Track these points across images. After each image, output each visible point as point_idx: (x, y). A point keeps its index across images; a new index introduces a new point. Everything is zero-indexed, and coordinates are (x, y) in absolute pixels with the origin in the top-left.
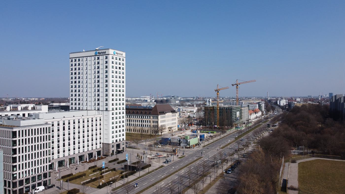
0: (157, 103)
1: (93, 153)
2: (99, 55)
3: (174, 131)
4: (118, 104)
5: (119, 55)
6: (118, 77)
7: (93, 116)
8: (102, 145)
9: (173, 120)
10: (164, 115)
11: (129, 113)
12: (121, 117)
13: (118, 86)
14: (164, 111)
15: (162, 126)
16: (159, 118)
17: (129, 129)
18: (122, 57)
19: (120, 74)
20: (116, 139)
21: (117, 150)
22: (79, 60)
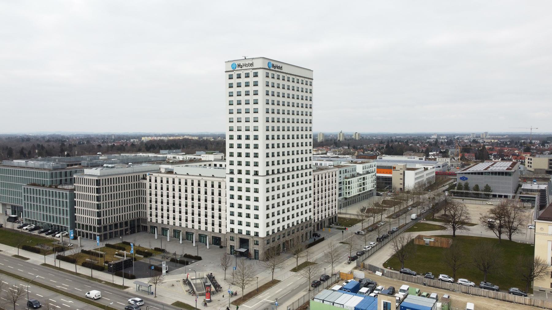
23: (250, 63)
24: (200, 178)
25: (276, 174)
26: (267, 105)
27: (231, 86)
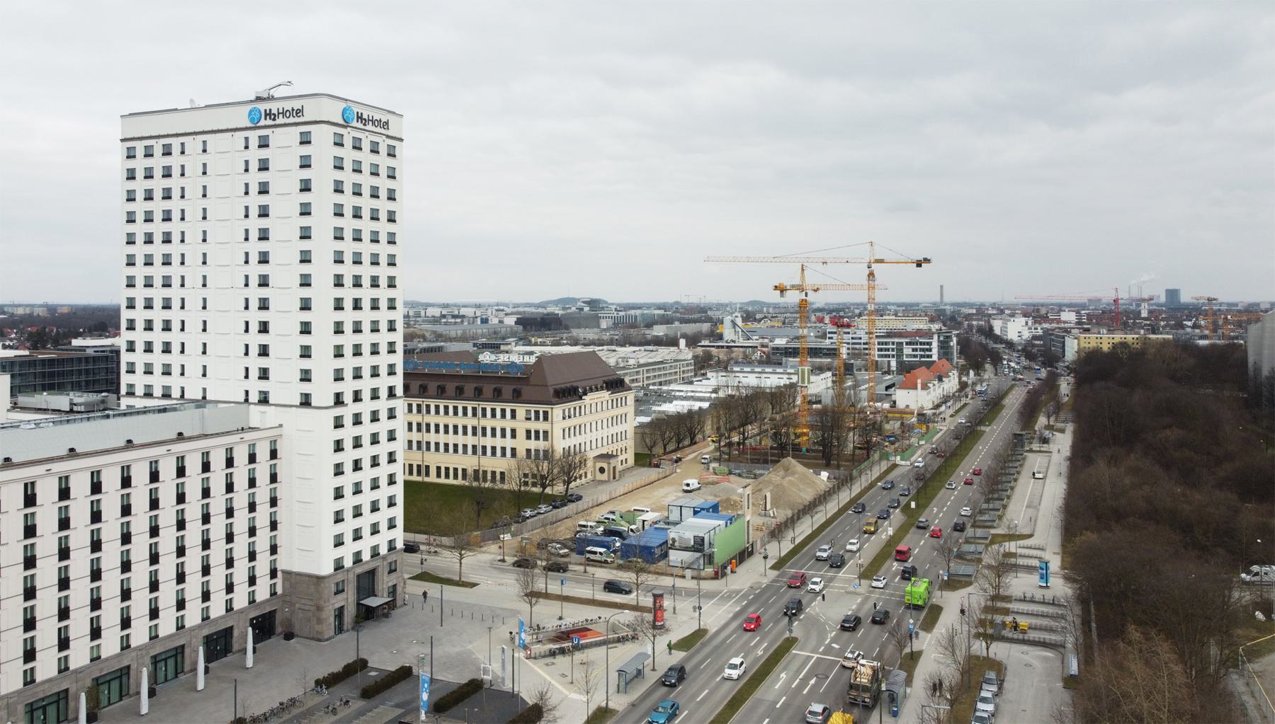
0: (525, 328)
1: (231, 628)
2: (269, 122)
3: (619, 468)
4: (366, 327)
5: (370, 127)
6: (366, 214)
7: (236, 438)
8: (284, 580)
9: (614, 420)
10: (577, 403)
11: (423, 392)
12: (383, 371)
13: (366, 259)
14: (575, 384)
15: (567, 453)
16: (555, 419)
17: (419, 466)
18: (388, 137)
19: (378, 175)
20: (357, 546)
21: (358, 604)
22: (167, 152)
23: (296, 109)
24: (179, 448)
25: (400, 397)
26: (338, 219)
27: (131, 176)
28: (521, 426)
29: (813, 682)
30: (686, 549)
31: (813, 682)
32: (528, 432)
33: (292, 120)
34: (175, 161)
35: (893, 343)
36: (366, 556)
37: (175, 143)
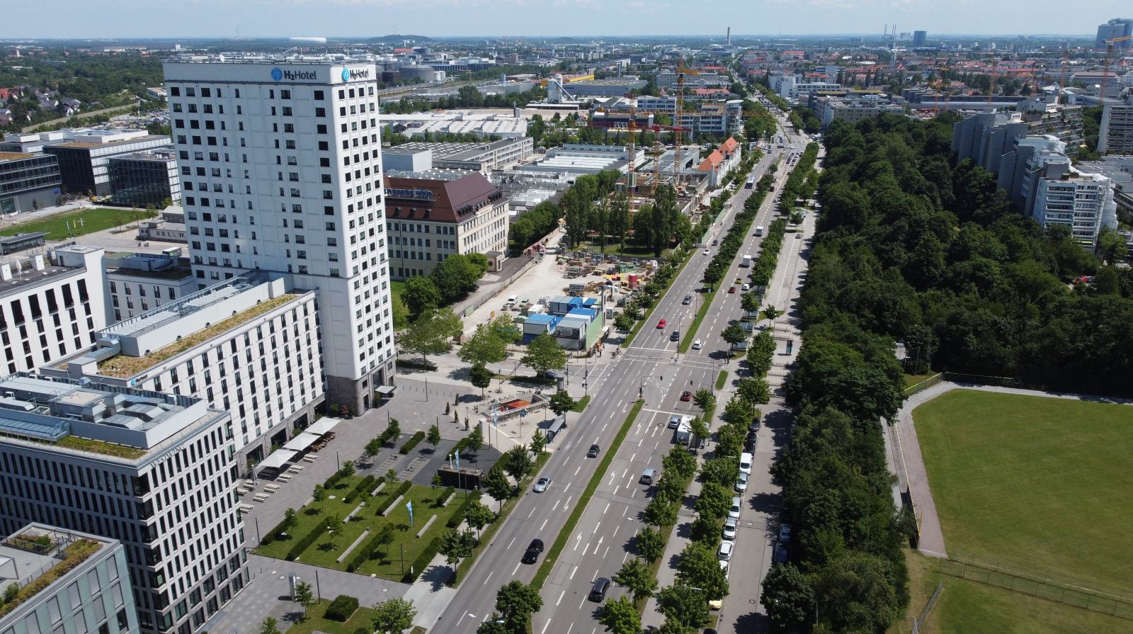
1: (306, 415)
14: (470, 203)
28: (434, 237)
29: (656, 429)
30: (567, 337)
31: (656, 429)
32: (439, 242)
33: (306, 81)
34: (212, 100)
35: (692, 118)
36: (377, 363)
37: (213, 89)
